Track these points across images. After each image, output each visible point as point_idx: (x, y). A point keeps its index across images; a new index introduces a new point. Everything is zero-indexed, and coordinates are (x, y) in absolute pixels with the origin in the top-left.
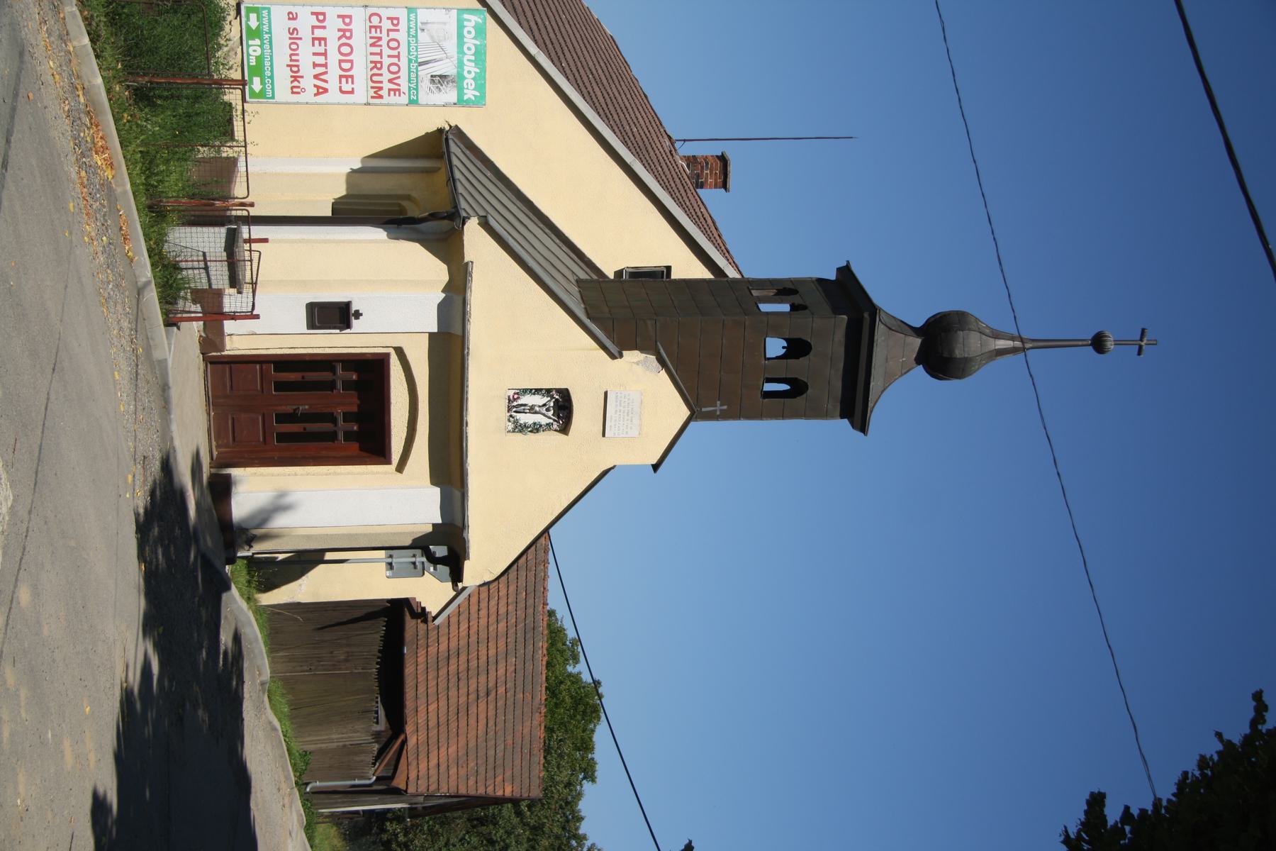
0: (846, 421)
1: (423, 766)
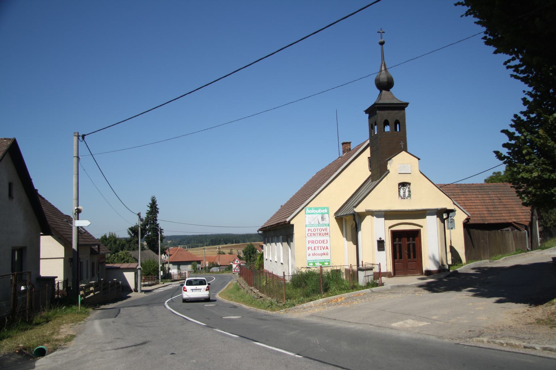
0: (406, 109)
1: (522, 217)
